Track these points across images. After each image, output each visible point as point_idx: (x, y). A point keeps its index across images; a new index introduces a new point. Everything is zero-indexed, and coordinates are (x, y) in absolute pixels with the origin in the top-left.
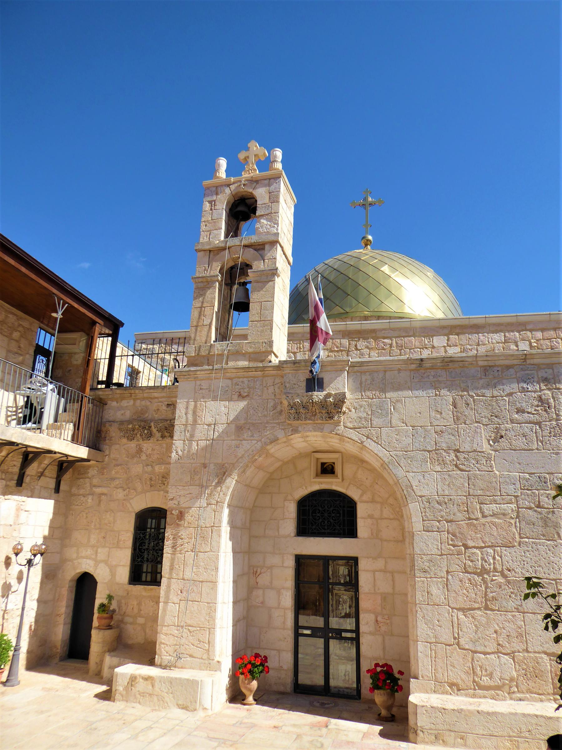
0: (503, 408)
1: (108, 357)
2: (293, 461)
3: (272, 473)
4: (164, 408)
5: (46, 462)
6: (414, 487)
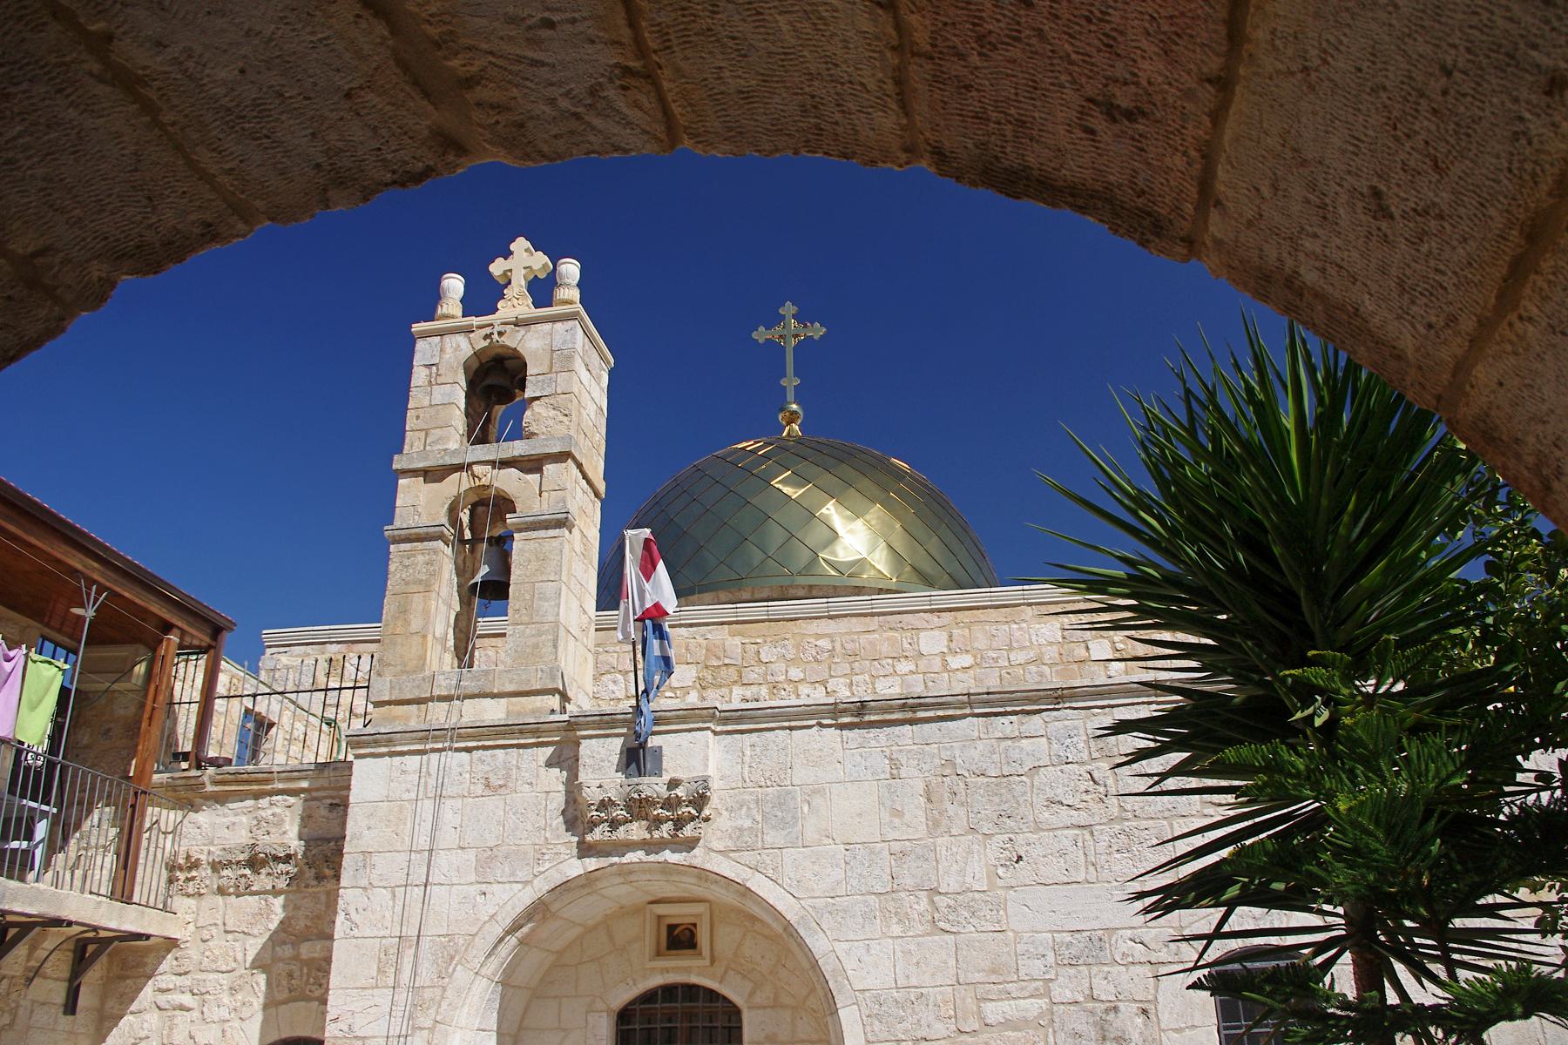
0: (1021, 800)
1: (197, 696)
2: (606, 924)
3: (560, 953)
4: (324, 812)
5: (49, 944)
6: (850, 973)
